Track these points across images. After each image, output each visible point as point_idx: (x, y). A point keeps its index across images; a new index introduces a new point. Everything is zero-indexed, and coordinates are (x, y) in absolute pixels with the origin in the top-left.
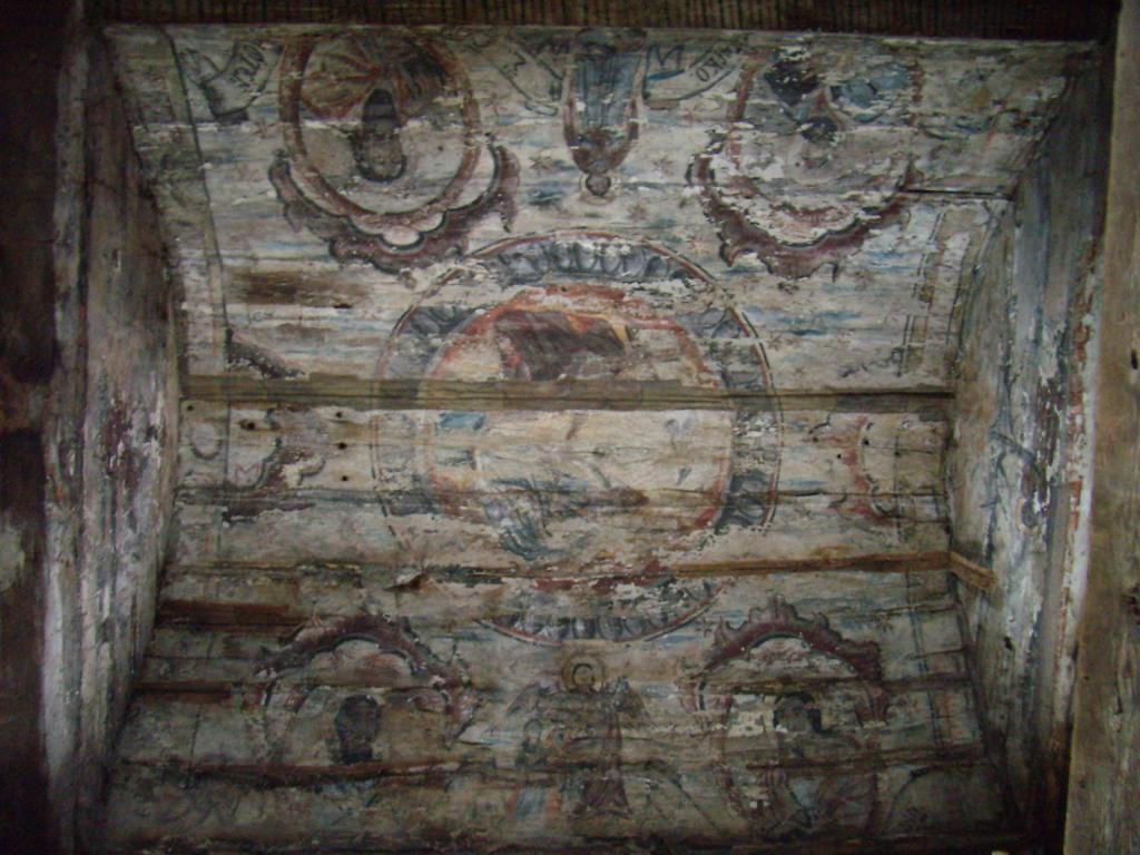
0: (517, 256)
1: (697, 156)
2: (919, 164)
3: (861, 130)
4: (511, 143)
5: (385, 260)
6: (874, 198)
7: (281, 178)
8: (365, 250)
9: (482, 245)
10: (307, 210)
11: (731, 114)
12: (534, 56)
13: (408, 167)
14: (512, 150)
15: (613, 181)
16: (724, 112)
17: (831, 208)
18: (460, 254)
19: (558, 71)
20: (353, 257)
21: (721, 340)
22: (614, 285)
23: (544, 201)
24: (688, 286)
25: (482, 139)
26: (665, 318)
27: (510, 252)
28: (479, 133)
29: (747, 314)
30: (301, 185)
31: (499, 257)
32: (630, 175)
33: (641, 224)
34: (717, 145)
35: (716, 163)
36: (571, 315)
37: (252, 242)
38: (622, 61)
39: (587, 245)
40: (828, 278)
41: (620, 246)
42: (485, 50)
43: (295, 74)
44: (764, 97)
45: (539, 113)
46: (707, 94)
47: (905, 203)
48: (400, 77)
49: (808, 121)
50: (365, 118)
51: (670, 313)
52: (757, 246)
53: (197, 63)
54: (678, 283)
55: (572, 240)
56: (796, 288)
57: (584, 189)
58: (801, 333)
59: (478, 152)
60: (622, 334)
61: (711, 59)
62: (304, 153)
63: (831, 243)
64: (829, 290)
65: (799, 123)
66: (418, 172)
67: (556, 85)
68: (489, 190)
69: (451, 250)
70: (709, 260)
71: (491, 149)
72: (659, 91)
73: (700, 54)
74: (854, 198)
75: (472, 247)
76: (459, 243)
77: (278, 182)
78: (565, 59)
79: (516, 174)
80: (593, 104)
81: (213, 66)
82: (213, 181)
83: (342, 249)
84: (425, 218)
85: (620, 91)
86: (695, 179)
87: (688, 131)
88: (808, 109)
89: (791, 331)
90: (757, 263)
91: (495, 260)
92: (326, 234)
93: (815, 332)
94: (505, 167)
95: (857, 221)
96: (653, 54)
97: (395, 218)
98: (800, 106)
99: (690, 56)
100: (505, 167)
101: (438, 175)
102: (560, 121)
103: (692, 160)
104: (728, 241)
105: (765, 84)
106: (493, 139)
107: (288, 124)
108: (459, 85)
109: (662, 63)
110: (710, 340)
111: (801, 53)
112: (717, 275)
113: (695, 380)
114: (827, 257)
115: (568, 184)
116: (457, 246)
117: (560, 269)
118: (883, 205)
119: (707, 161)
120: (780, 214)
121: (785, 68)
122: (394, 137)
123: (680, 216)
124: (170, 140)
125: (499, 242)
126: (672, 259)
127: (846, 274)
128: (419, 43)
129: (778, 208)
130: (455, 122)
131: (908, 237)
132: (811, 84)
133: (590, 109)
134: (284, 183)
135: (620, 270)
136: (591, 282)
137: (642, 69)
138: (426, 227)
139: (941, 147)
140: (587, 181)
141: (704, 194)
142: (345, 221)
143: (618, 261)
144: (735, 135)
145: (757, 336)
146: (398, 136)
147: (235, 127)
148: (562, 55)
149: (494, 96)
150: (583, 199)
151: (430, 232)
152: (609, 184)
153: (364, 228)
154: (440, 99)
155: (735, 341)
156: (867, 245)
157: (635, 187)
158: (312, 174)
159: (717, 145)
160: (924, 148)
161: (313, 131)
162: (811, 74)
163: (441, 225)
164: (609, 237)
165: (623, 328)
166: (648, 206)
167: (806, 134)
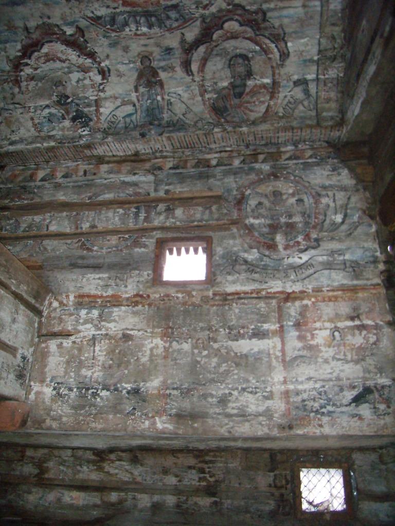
0: (177, 20)
1: (108, 80)
2: (16, 90)
3: (47, 102)
4: (185, 78)
5: (239, 12)
6: (28, 71)
7: (284, 53)
8: (249, 17)
10: (274, 37)
12: (180, 118)
13: (228, 62)
14: (184, 75)
16: (103, 103)
17: (44, 63)
18: (203, 17)
19: (170, 112)
20: (254, 13)
22: (128, 9)
23: (169, 50)
25: (197, 79)
27: (180, 22)
28: (198, 82)
30: (276, 50)
31: (185, 20)
32: (133, 68)
34: (101, 87)
35: (99, 78)
37: (302, 16)
38: (146, 119)
41: (130, 31)
42: (198, 119)
43: (272, 103)
44: (90, 111)
45: (175, 93)
46: (111, 110)
48: (231, 105)
49: (69, 103)
50: (245, 85)
53: (309, 105)
54: (99, 14)
55: (152, 31)
57: (151, 58)
59: (198, 73)
62: (272, 67)
65: (72, 101)
66: (224, 60)
68: (193, 54)
69: (208, 21)
70: (87, 27)
71: (193, 75)
72: (129, 109)
74: (36, 69)
75: (198, 23)
76: (204, 25)
77: (286, 51)
78: (168, 118)
79: (182, 63)
80: (154, 99)
81: (303, 105)
82: (315, 50)
83: (260, 17)
84: (220, 37)
85: (145, 107)
86: (106, 69)
87: (114, 92)
90: (65, 28)
91: (187, 17)
92: (267, 24)
94: (186, 65)
95: (30, 58)
96: (135, 124)
97: (234, 36)
98: (75, 109)
99: (121, 125)
100: (186, 65)
101: (215, 59)
102: (166, 90)
104: (82, 39)
106: (193, 79)
107: (277, 80)
108: (207, 103)
111: (82, 132)
112: (81, 20)
115: (159, 60)
116: (205, 23)
118: (22, 68)
119: (103, 79)
121: (85, 125)
122: (233, 77)
123: (107, 51)
124: (329, 69)
125: (187, 26)
128: (223, 120)
129: (67, 59)
133: (155, 97)
134: (283, 51)
135: (127, 18)
136: (140, 9)
137: (138, 117)
138: (220, 32)
140: (151, 62)
141: (100, 63)
142: (258, 33)
143: (130, 22)
144: (95, 93)
146: (232, 78)
147: (300, 78)
148: (169, 119)
149: (193, 99)
150: (151, 53)
151: (217, 30)
152: (141, 62)
153: (249, 29)
154: (215, 96)
158: (270, 56)
160: (19, 98)
161: (267, 78)
163: (213, 33)
164: (136, 35)
167: (68, 97)
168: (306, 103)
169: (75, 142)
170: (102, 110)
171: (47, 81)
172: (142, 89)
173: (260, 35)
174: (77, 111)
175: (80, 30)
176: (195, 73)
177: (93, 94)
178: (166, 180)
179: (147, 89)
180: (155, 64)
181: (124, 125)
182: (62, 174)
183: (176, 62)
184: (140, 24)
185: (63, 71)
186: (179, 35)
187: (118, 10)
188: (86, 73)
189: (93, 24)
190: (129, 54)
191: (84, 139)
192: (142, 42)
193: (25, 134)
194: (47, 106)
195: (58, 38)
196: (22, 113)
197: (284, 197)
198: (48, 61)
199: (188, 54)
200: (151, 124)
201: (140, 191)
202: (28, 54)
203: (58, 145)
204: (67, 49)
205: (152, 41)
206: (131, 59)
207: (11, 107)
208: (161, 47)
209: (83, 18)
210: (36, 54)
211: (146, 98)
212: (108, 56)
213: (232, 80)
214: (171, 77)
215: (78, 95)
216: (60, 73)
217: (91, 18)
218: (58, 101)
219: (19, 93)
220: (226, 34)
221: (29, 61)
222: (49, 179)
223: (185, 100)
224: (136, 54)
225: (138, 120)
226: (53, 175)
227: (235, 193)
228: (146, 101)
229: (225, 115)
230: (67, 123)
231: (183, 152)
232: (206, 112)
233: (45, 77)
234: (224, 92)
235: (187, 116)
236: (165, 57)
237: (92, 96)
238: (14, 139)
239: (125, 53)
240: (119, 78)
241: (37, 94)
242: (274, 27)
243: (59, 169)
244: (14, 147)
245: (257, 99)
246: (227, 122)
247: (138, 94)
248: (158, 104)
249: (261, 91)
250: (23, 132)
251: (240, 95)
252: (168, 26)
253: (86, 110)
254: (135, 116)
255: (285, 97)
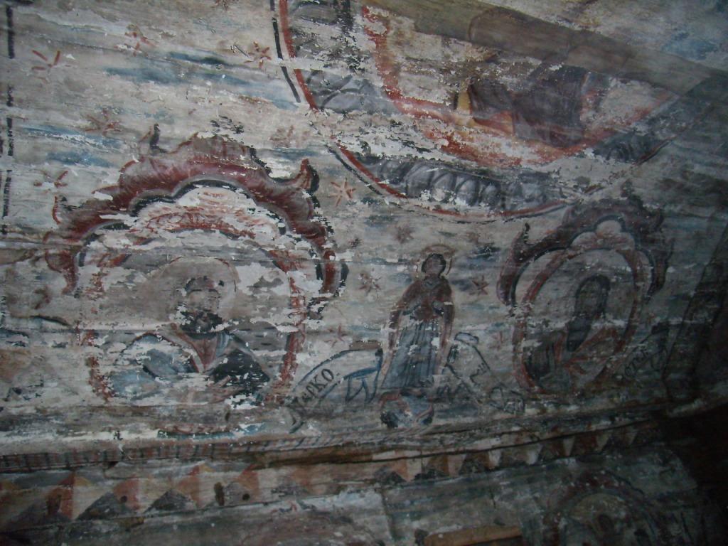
2: (60, 283)
3: (153, 326)
6: (116, 241)
9: (553, 213)
11: (300, 339)
15: (420, 269)
19: (448, 371)
21: (338, 71)
24: (365, 145)
25: (518, 312)
26: (404, 112)
29: (293, 99)
32: (402, 274)
33: (402, 224)
34: (315, 308)
35: (313, 287)
36: (507, 133)
39: (461, 203)
40: (165, 131)
44: (268, 358)
45: (469, 334)
46: (320, 359)
47: (67, 233)
48: (556, 361)
49: (214, 334)
50: (588, 328)
51: (394, 117)
52: (270, 185)
54: (376, 150)
56: (216, 124)
58: (213, 61)
59: (525, 300)
60: (463, 101)
61: (320, 390)
63: (172, 185)
64: (165, 115)
65: (226, 331)
67: (452, 360)
70: (332, 172)
71: (514, 303)
72: (366, 359)
73: (330, 394)
76: (571, 218)
77: (660, 280)
86: (338, 268)
88: (218, 347)
89: (226, 65)
91: (551, 198)
93: (186, 57)
94: (508, 284)
95: (134, 214)
96: (371, 392)
98: (228, 351)
100: (508, 284)
101: (560, 279)
103: (342, 290)
104: (306, 195)
105: (268, 371)
109: (364, 385)
110: (356, 77)
113: (393, 23)
114: (170, 162)
117: (497, 185)
119: (324, 290)
120: (240, 227)
121: (248, 388)
123: (359, 230)
126: (377, 180)
127: (138, 134)
128: (536, 388)
129: (244, 233)
130: (533, 327)
131: (49, 186)
132: (218, 374)
133: (428, 339)
135: (437, 175)
136: (474, 165)
137: (381, 378)
139: (37, 307)
140: (443, 269)
141: (329, 253)
144: (297, 319)
145: (284, 69)
149: (499, 348)
152: (424, 265)
154: (537, 345)
155: (319, 66)
156: (112, 179)
157: (401, 261)
159: (315, 308)
160: (60, 305)
161: (622, 318)
162: (221, 383)
164: (438, 209)
165: (459, 108)
166: (392, 243)
167: (218, 320)
168: (656, 360)
169: (218, 433)
170: (300, 358)
171: (166, 273)
172: (407, 322)
173: (641, 250)
174: (234, 355)
175: (311, 177)
176: (519, 301)
177: (290, 321)
178: (407, 502)
179: (418, 323)
180: (449, 274)
181: (343, 393)
182: (153, 497)
183: (492, 276)
184: (457, 191)
185: (221, 256)
186: (521, 228)
187: (427, 156)
188: (285, 269)
189: (350, 169)
190: (405, 246)
191: (243, 426)
192: (445, 227)
193: (57, 400)
194: (150, 335)
195: (241, 181)
196: (61, 346)
197: (617, 526)
198: (192, 227)
199: (518, 263)
200: (405, 393)
201: (363, 538)
202: (133, 202)
203: (167, 438)
204: (258, 209)
205: (464, 228)
206: (405, 257)
207: (30, 325)
208: (477, 243)
209: (331, 150)
210: (159, 205)
211: (409, 339)
212: (356, 243)
213: (573, 319)
214: (471, 304)
215: (248, 318)
216: (210, 259)
217: (351, 156)
218: (185, 327)
219: (65, 292)
220: (596, 240)
221: (128, 220)
222: (112, 513)
223: (483, 348)
224: (419, 249)
225: (379, 385)
226: (124, 499)
227: (543, 528)
228: (408, 346)
229: (542, 378)
230: (198, 381)
231: (441, 441)
232: (514, 372)
233: (162, 263)
234: (554, 339)
235: (479, 379)
236: (475, 262)
237: (283, 324)
238: (14, 411)
239: (397, 242)
240: (364, 291)
241: (123, 304)
242: (663, 241)
243: (142, 481)
244: (18, 439)
245: (597, 353)
246: (543, 392)
247: (395, 331)
248: (430, 353)
249: (607, 339)
250: (52, 394)
251: (573, 346)
252: (508, 208)
253: (259, 354)
254: (373, 375)
255: (635, 350)
